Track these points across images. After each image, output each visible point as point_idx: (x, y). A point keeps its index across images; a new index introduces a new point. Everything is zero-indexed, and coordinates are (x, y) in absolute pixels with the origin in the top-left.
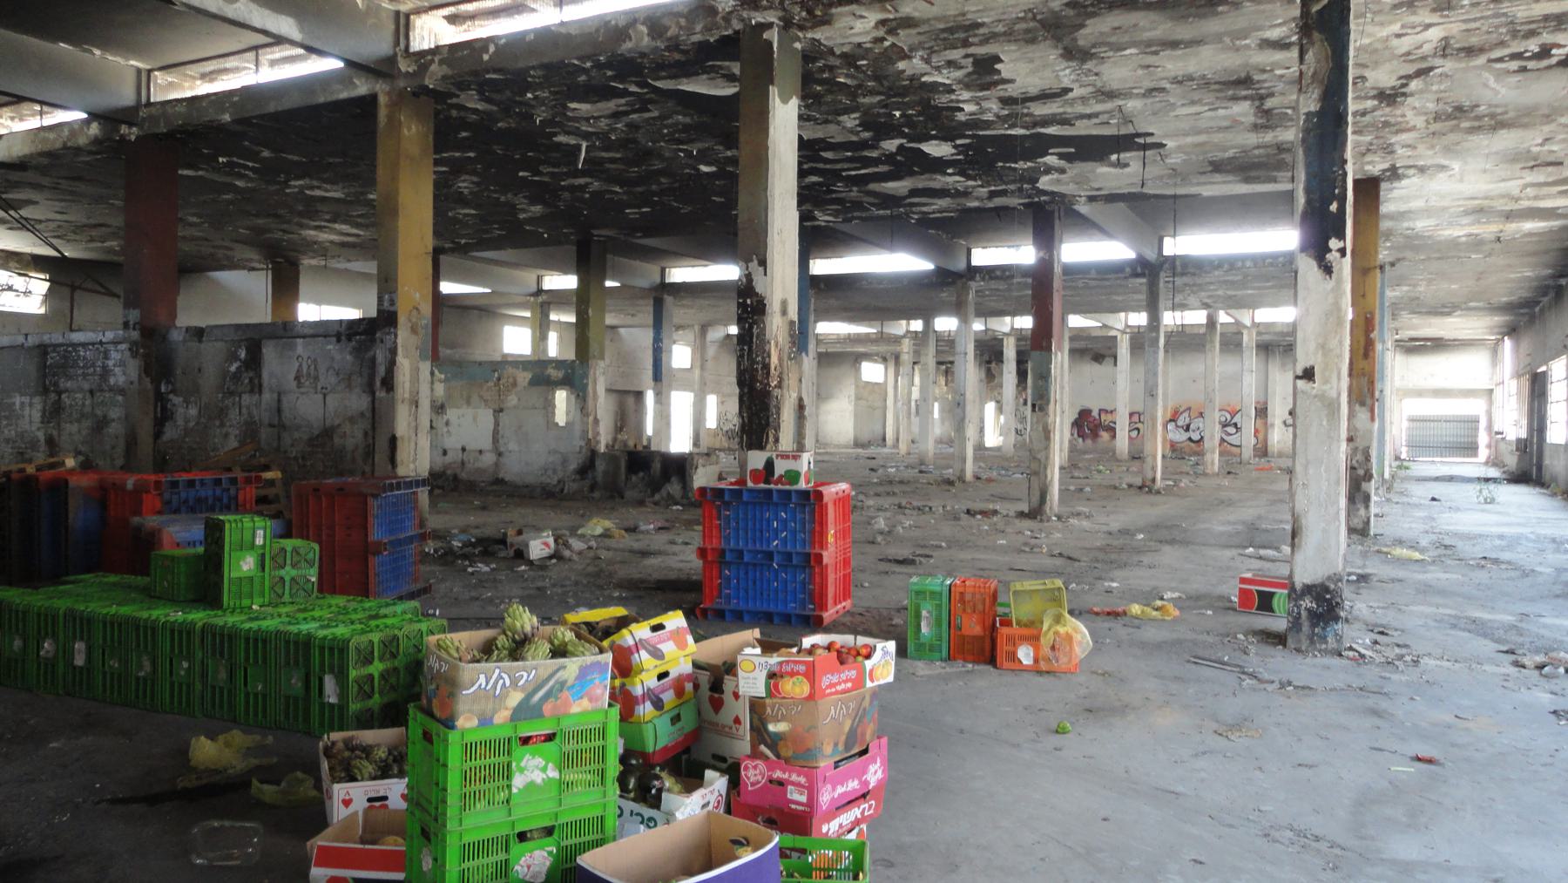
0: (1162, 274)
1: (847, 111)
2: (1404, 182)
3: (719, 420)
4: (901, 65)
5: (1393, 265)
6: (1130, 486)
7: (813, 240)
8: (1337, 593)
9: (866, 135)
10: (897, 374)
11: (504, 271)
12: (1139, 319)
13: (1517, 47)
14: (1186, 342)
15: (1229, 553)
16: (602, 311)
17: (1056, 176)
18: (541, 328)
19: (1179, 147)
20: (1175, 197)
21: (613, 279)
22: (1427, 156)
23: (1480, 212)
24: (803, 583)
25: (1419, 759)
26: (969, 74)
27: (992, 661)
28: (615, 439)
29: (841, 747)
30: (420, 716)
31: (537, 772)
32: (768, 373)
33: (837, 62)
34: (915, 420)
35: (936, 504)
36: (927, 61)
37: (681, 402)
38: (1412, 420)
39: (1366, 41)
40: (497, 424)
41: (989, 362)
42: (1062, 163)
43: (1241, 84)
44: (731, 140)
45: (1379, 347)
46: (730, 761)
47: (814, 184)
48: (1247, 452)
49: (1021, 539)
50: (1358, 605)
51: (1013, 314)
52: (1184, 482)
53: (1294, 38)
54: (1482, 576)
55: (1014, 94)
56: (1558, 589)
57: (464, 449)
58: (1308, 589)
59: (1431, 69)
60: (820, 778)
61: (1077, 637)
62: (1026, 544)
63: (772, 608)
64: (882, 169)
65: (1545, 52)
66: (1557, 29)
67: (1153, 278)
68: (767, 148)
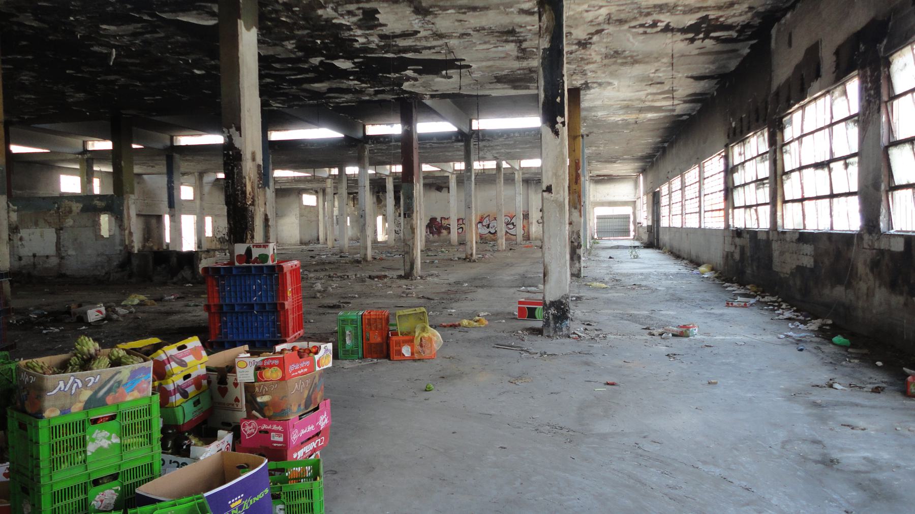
0: (472, 140)
1: (288, 38)
2: (592, 91)
3: (213, 231)
4: (320, 12)
5: (587, 135)
6: (459, 258)
7: (271, 119)
8: (566, 305)
9: (300, 54)
10: (324, 201)
11: (59, 138)
12: (460, 166)
13: (642, 21)
14: (486, 178)
15: (512, 290)
16: (131, 164)
17: (412, 82)
18: (87, 176)
19: (479, 68)
20: (477, 96)
21: (138, 144)
22: (603, 77)
23: (627, 108)
24: (273, 322)
25: (608, 384)
26: (360, 20)
27: (388, 356)
28: (144, 246)
29: (302, 407)
30: (15, 414)
31: (104, 441)
32: (245, 197)
33: (280, 8)
34: (336, 227)
35: (351, 274)
36: (336, 10)
37: (188, 222)
38: (599, 218)
39: (571, 13)
40: (58, 238)
41: (378, 192)
42: (416, 75)
43: (508, 34)
44: (214, 54)
45: (582, 179)
46: (233, 425)
47: (268, 83)
48: (520, 238)
49: (400, 290)
50: (576, 312)
51: (390, 164)
52: (488, 255)
53: (536, 9)
54: (633, 293)
55: (387, 33)
56: (667, 297)
57: (34, 256)
58: (553, 304)
59: (603, 30)
60: (291, 426)
61: (435, 338)
62: (403, 292)
63: (255, 338)
64: (311, 75)
65: (654, 24)
66: (660, 12)
67: (467, 142)
68: (238, 58)
